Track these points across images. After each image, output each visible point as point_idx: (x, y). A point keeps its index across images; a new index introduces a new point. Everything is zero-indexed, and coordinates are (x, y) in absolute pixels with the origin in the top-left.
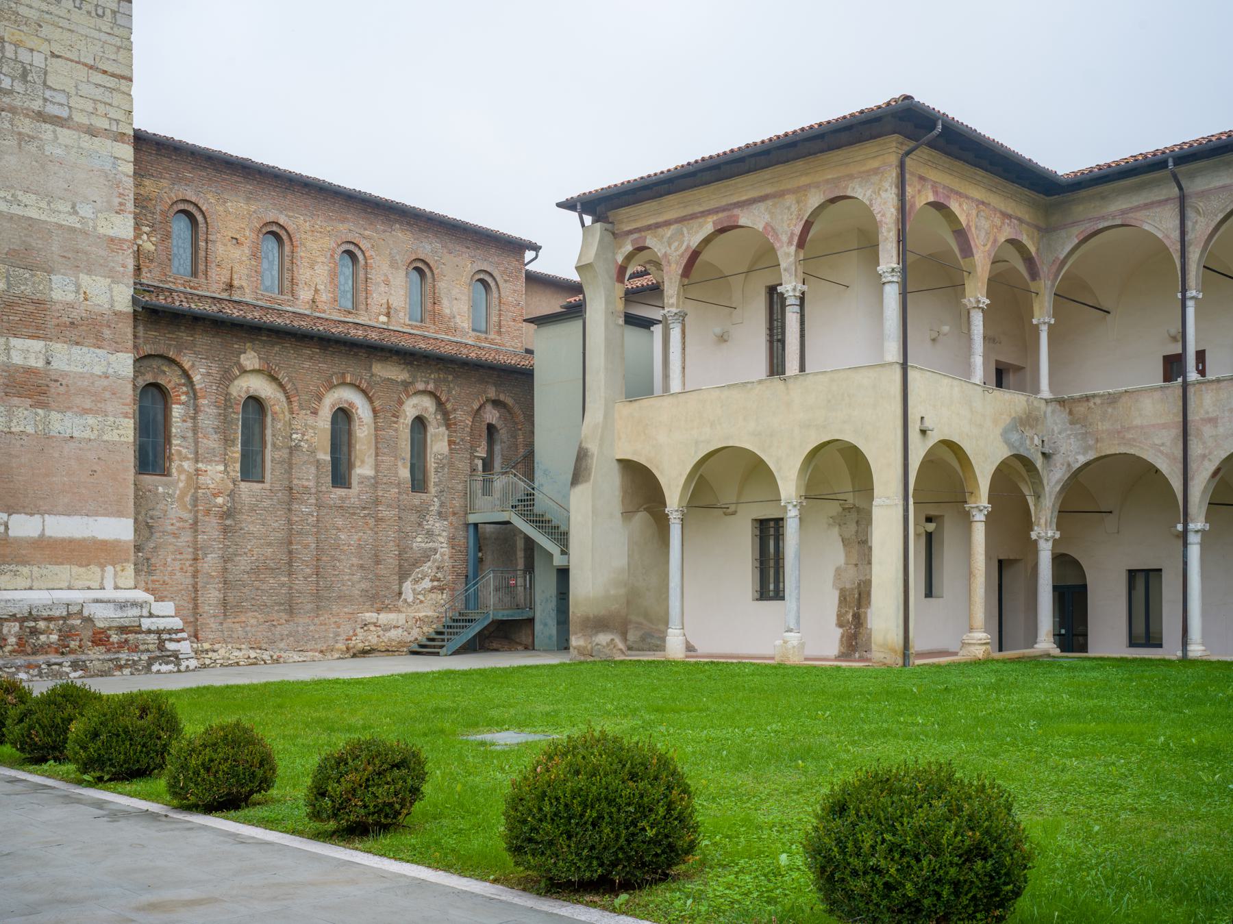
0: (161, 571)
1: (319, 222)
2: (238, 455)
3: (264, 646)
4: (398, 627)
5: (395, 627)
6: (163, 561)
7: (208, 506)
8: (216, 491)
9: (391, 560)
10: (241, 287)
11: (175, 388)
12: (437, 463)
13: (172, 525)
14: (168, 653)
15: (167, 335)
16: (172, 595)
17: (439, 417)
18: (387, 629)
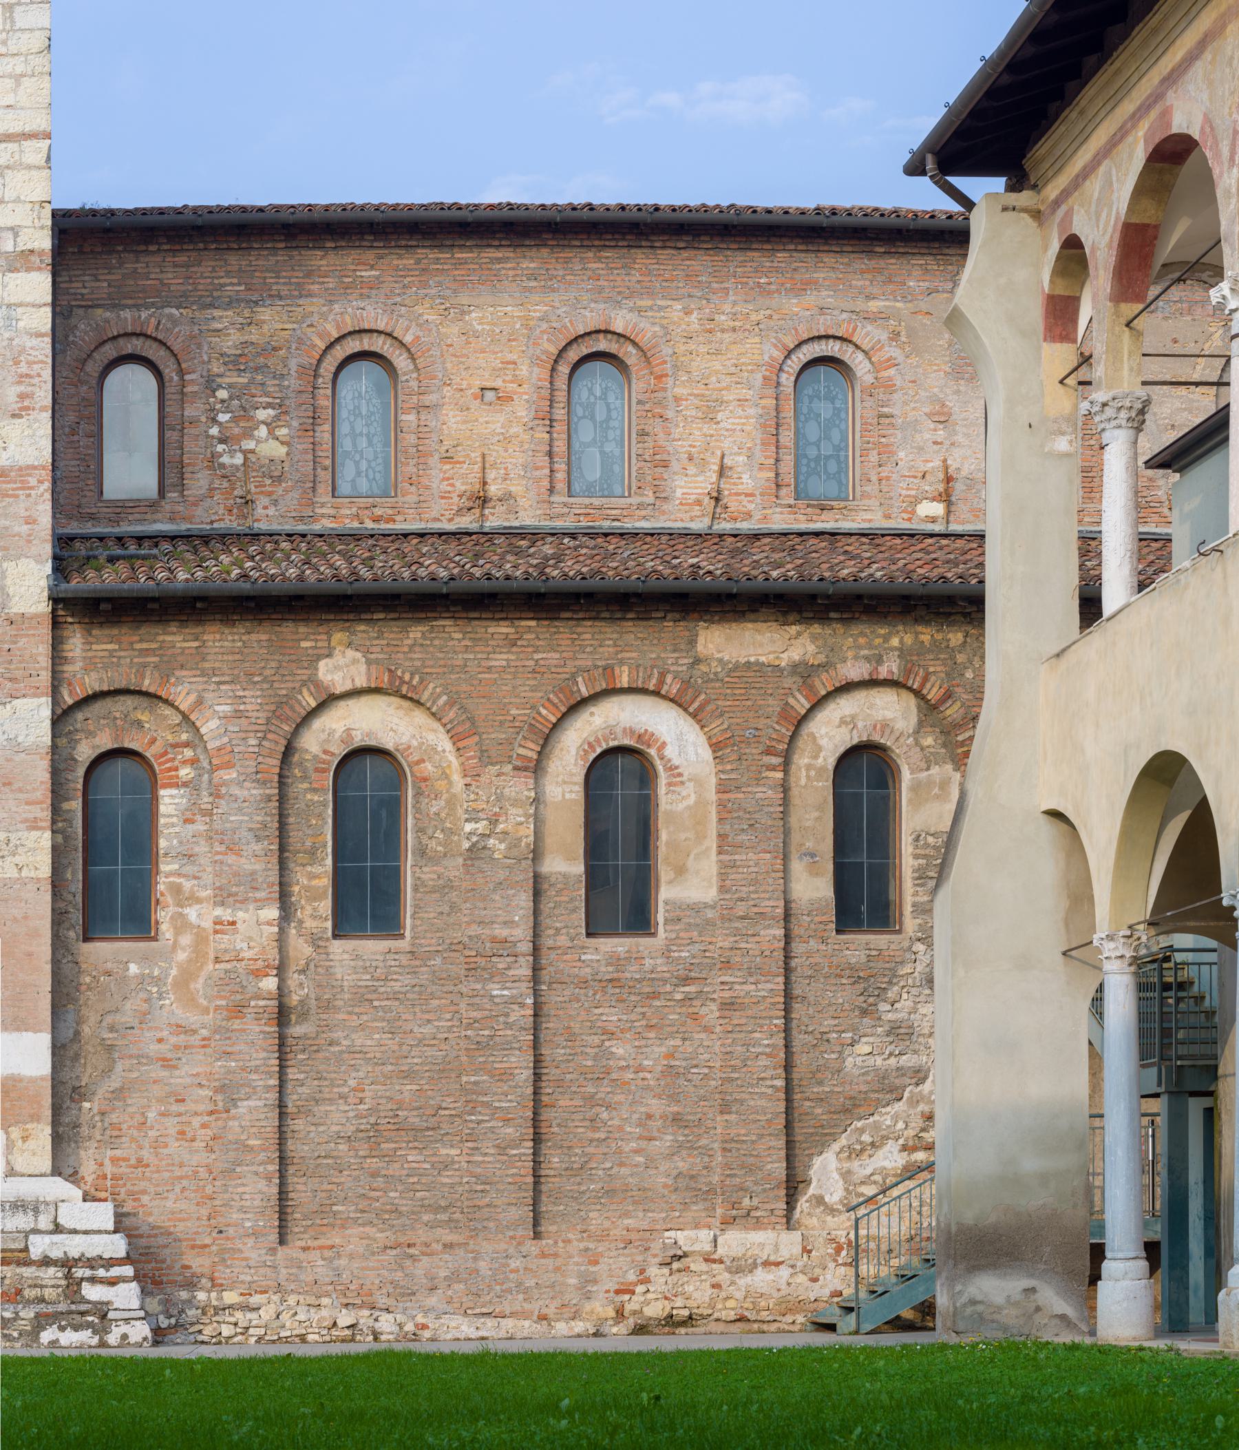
0: (133, 1139)
1: (727, 308)
2: (325, 882)
3: (382, 1301)
4: (778, 1264)
5: (766, 1264)
6: (139, 1118)
7: (239, 997)
8: (260, 964)
9: (763, 1103)
10: (507, 497)
11: (166, 753)
12: (925, 856)
13: (160, 1041)
14: (83, 1307)
15: (138, 646)
16: (160, 1189)
17: (929, 741)
18: (741, 1266)
